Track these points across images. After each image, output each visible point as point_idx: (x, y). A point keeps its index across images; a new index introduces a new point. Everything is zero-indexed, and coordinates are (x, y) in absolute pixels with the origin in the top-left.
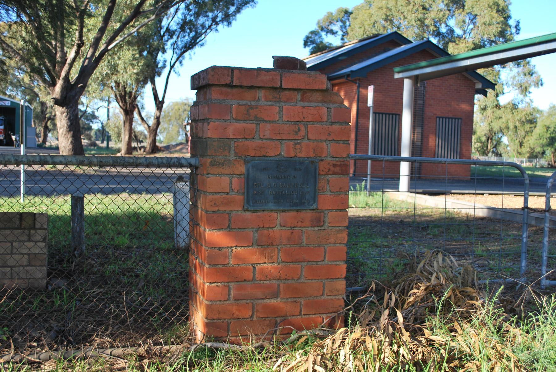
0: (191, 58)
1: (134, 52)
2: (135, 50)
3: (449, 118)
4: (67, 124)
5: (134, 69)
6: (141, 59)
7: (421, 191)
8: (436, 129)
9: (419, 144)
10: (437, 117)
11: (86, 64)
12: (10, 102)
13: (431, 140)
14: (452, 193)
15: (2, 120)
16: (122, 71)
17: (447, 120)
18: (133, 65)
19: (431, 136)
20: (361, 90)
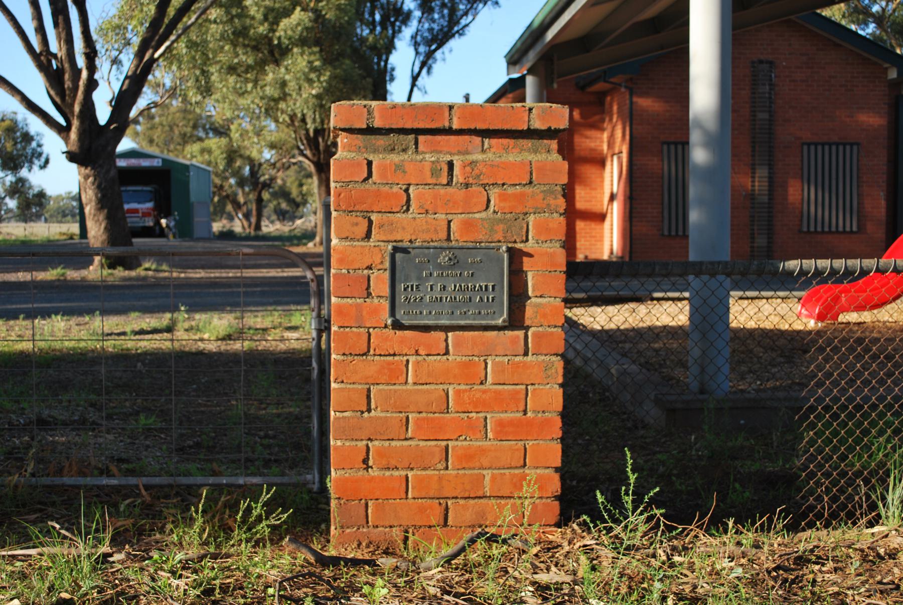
0: (444, 60)
1: (312, 58)
2: (314, 53)
3: (830, 145)
4: (96, 196)
5: (313, 88)
6: (325, 70)
7: (271, 300)
8: (802, 169)
9: (765, 199)
10: (803, 144)
11: (124, 88)
12: (160, 160)
13: (791, 190)
14: (653, 299)
15: (150, 191)
16: (294, 95)
17: (827, 148)
18: (310, 81)
19: (792, 182)
20: (635, 99)
